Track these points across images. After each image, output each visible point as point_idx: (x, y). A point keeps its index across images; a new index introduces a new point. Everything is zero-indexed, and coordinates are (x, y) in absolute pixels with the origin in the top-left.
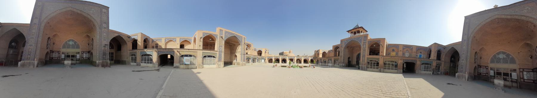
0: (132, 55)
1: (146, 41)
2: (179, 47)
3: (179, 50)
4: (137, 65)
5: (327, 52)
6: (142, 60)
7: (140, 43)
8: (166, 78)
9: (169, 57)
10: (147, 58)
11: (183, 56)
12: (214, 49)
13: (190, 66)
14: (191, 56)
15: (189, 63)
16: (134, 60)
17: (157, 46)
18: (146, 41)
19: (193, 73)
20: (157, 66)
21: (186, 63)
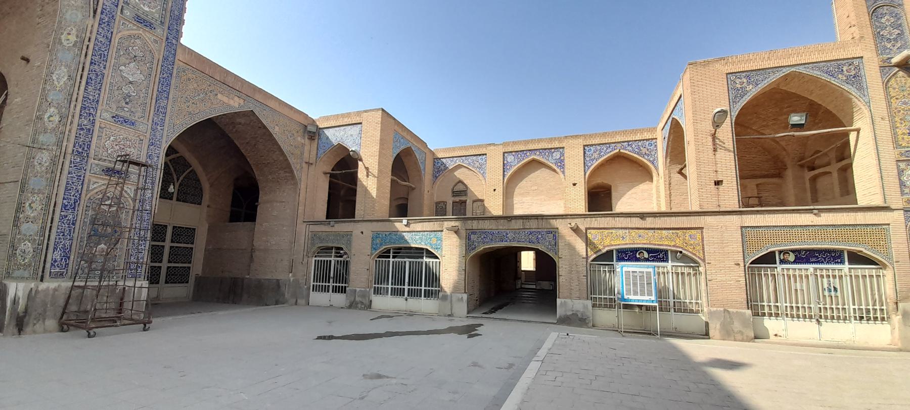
0: (327, 250)
1: (404, 164)
2: (580, 205)
3: (582, 224)
4: (352, 305)
5: (200, 274)
6: (381, 278)
7: (372, 181)
8: (514, 372)
9: (528, 262)
10: (409, 271)
11: (606, 257)
12: (847, 189)
13: (658, 320)
14: (657, 255)
15: (649, 299)
16: (334, 276)
17: (459, 205)
18: (404, 164)
19: (684, 360)
20: (461, 308)
21: (635, 298)
